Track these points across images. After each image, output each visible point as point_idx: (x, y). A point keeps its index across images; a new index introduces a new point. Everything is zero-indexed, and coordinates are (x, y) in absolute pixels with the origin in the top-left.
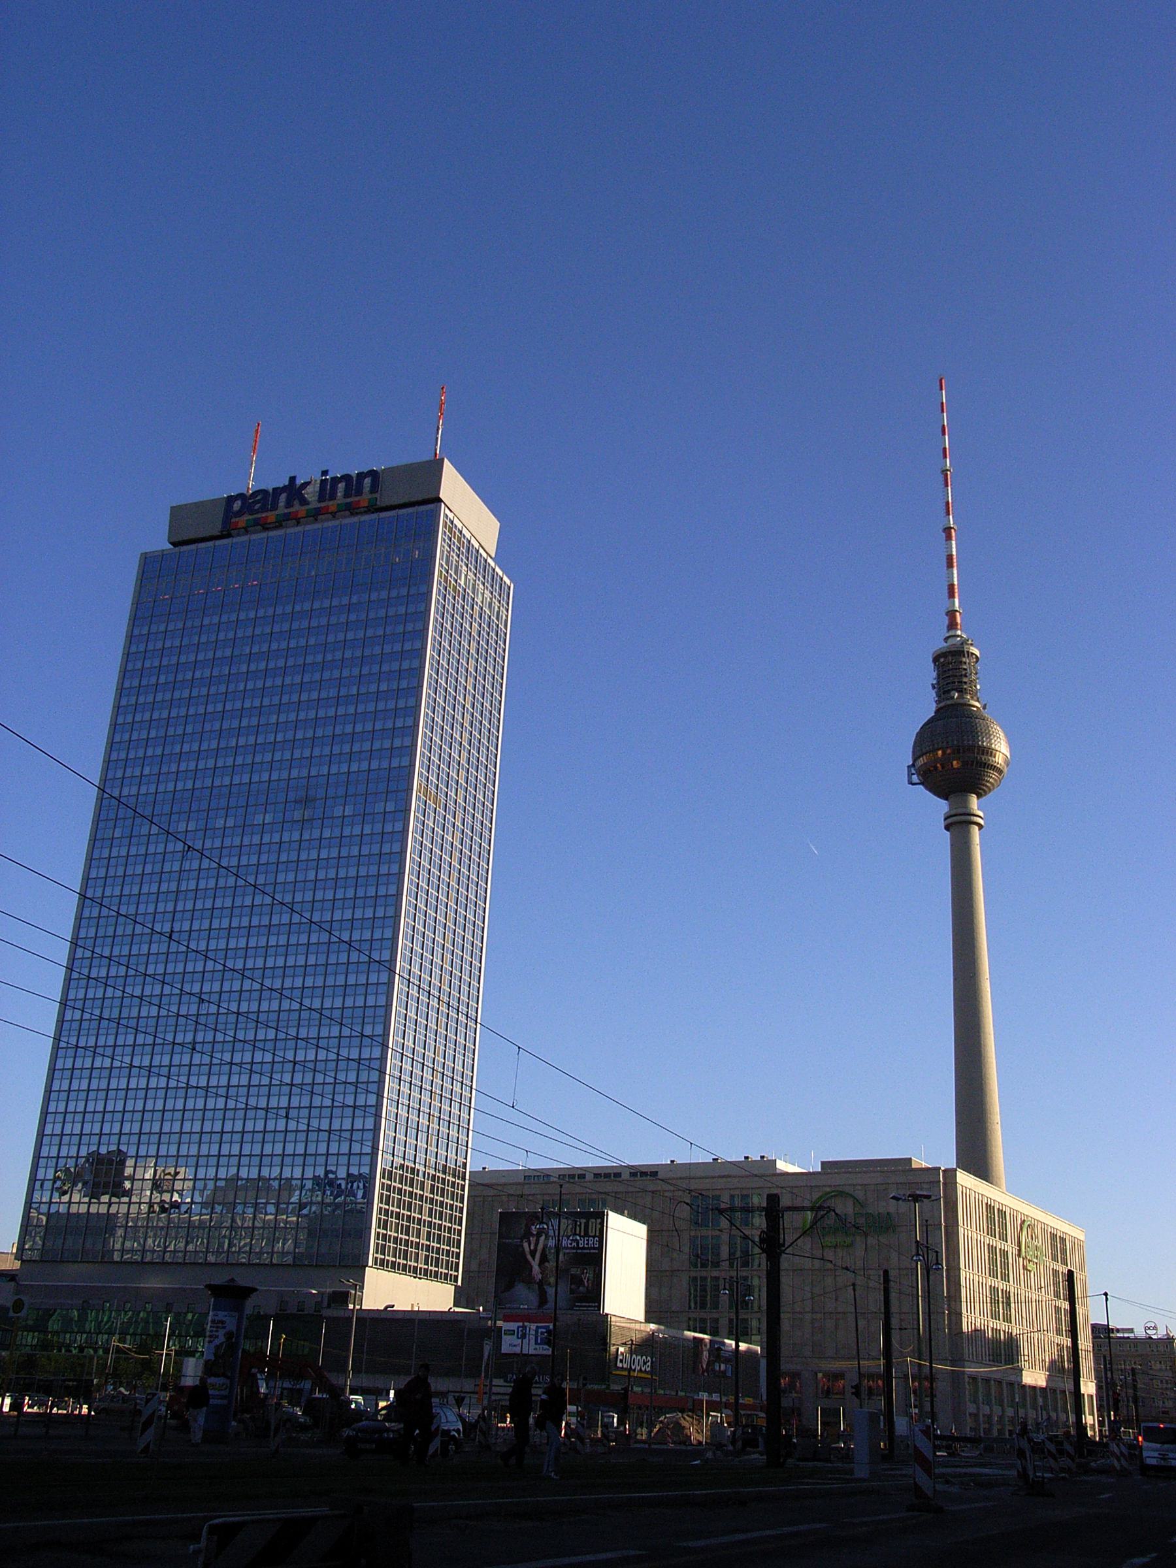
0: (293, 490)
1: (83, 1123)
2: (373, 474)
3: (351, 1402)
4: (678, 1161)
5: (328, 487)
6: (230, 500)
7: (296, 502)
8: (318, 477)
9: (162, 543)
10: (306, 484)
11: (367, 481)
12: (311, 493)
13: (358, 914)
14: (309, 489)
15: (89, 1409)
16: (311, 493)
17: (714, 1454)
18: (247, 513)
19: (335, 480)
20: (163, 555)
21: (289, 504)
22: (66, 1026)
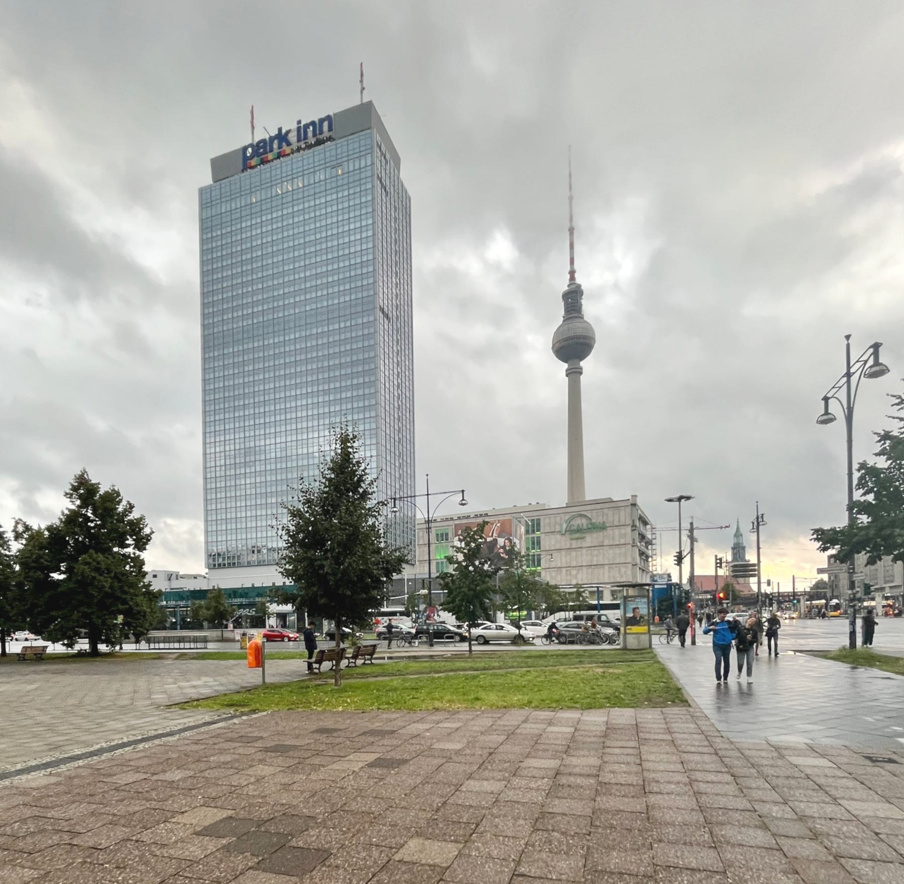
0: (282, 137)
1: (430, 560)
2: (328, 118)
3: (227, 620)
4: (876, 627)
5: (302, 131)
6: (245, 149)
7: (284, 144)
8: (294, 126)
9: (208, 180)
10: (288, 132)
11: (326, 124)
12: (293, 137)
13: (288, 394)
14: (290, 135)
15: (57, 570)
16: (293, 137)
17: (84, 539)
18: (261, 153)
19: (306, 126)
20: (210, 187)
21: (280, 147)
22: (208, 456)
